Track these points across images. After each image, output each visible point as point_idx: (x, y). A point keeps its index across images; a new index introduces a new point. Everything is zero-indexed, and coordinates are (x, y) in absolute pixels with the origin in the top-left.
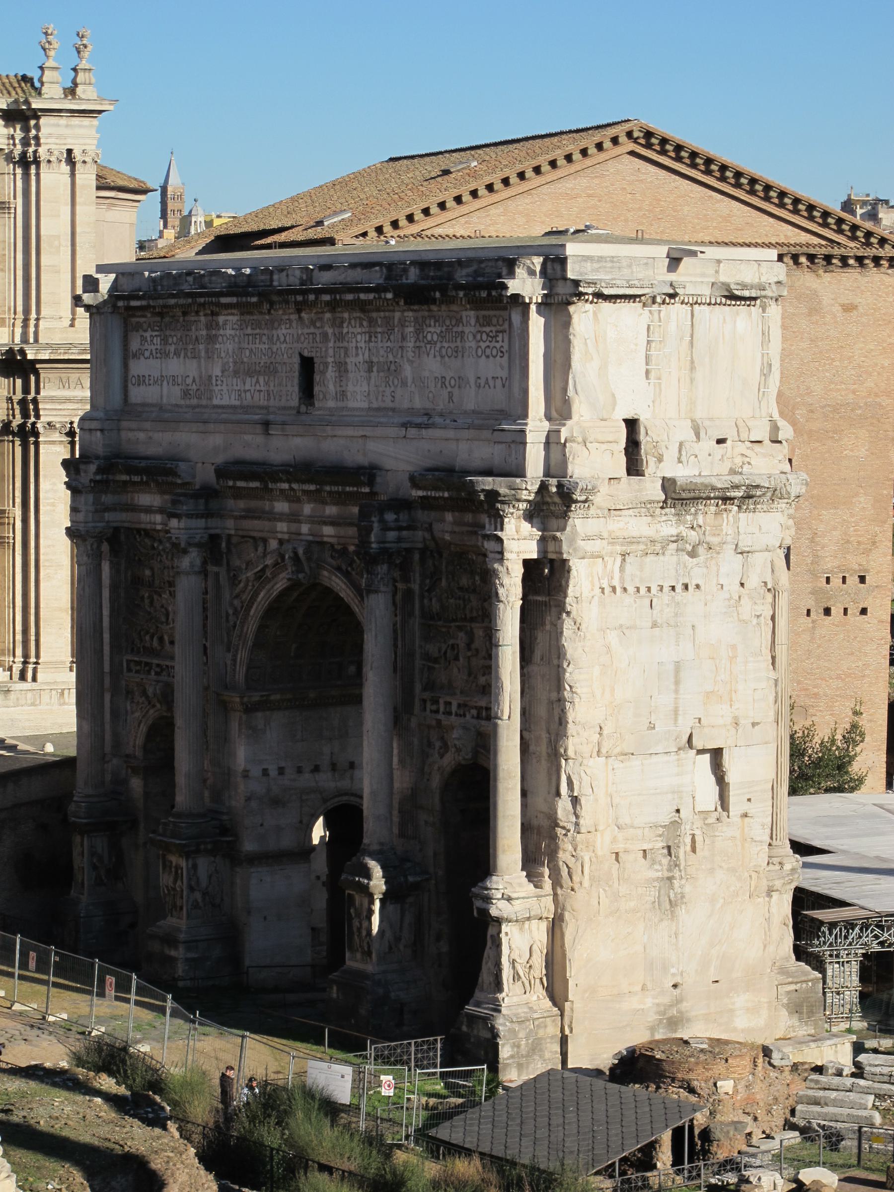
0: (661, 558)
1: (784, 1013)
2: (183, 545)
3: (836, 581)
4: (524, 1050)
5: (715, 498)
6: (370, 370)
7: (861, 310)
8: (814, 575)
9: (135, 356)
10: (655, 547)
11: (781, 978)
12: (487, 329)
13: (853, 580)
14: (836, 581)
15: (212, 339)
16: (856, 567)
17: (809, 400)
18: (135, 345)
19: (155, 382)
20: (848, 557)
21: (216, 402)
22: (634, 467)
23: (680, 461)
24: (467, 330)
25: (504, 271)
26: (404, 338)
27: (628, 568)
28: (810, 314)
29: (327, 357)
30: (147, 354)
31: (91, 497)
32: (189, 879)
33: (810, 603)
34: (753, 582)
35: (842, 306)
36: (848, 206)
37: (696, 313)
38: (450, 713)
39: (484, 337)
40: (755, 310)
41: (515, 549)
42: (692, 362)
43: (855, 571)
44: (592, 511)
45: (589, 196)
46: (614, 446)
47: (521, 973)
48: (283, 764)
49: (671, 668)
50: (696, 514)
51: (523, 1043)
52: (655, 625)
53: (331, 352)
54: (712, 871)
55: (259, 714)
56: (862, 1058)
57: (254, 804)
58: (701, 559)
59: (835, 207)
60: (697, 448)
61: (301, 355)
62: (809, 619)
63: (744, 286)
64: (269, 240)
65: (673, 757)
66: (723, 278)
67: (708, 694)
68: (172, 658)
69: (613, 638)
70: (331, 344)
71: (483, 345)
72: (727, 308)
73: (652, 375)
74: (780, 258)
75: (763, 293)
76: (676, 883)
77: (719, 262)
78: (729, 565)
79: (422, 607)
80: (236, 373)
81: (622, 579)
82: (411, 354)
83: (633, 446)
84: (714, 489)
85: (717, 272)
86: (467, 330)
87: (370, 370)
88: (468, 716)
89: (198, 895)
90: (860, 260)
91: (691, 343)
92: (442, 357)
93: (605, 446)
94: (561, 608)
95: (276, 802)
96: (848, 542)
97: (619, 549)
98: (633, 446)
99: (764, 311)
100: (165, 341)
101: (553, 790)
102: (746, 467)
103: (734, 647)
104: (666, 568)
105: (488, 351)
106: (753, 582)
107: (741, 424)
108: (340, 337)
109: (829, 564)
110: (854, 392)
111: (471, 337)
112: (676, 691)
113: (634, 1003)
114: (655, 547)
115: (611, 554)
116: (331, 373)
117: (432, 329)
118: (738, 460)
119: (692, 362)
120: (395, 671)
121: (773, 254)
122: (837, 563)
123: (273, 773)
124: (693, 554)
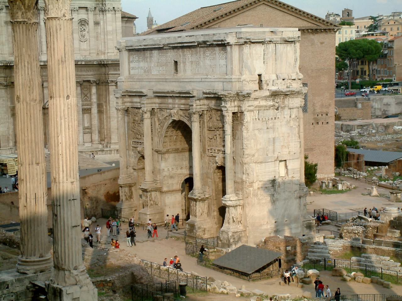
0: (269, 111)
1: (305, 229)
2: (145, 111)
3: (320, 116)
4: (236, 240)
5: (282, 95)
6: (192, 64)
7: (325, 43)
8: (314, 114)
9: (131, 62)
10: (268, 108)
11: (150, 237)
12: (222, 52)
13: (324, 115)
14: (320, 116)
15: (151, 57)
16: (325, 112)
17: (311, 68)
18: (131, 59)
19: (137, 69)
20: (323, 109)
21: (153, 73)
22: (261, 88)
23: (273, 85)
24: (217, 52)
25: (226, 36)
26: (200, 55)
27: (260, 114)
28: (312, 45)
29: (180, 60)
30: (134, 61)
31: (121, 99)
32: (149, 198)
33: (313, 121)
34: (293, 116)
35: (320, 42)
36: (328, 15)
37: (276, 46)
38: (215, 153)
39: (221, 54)
40: (293, 45)
41: (230, 110)
42: (276, 59)
43: (325, 113)
44: (251, 99)
45: (252, 16)
46: (255, 82)
47: (235, 220)
48: (173, 167)
49: (272, 139)
50: (278, 99)
51: (236, 238)
52: (267, 128)
53: (182, 59)
54: (284, 192)
55: (166, 155)
56: (326, 240)
57: (166, 178)
58: (279, 110)
59: (324, 17)
60: (277, 82)
61: (174, 61)
62: (313, 126)
63: (289, 38)
64: (169, 31)
65: (274, 163)
66: (284, 36)
67: (282, 146)
68: (143, 140)
69: (257, 132)
70: (182, 57)
71: (221, 56)
72: (285, 44)
73: (265, 63)
74: (299, 30)
75: (295, 40)
76: (275, 195)
77: (283, 32)
78: (287, 112)
79: (207, 125)
80: (157, 66)
81: (258, 117)
82: (202, 59)
83: (260, 81)
84: (282, 92)
85: (282, 34)
86: (217, 52)
87: (192, 64)
88: (220, 153)
89: (152, 202)
90: (325, 30)
91: (276, 54)
92: (210, 60)
93: (253, 82)
94: (242, 124)
95: (172, 177)
96: (323, 105)
97: (257, 109)
98: (260, 81)
99: (295, 44)
100: (139, 58)
101: (242, 172)
102: (291, 86)
103: (288, 133)
104: (271, 113)
105: (222, 58)
106: (293, 116)
107: (289, 75)
108: (184, 55)
109: (318, 110)
110: (324, 65)
111: (217, 54)
112: (274, 146)
113: (265, 227)
114: (268, 108)
115: (255, 110)
116: (182, 65)
117: (207, 53)
118: (289, 85)
119: (276, 59)
120: (201, 142)
121: (297, 29)
122: (320, 111)
123: (170, 170)
124: (277, 109)
